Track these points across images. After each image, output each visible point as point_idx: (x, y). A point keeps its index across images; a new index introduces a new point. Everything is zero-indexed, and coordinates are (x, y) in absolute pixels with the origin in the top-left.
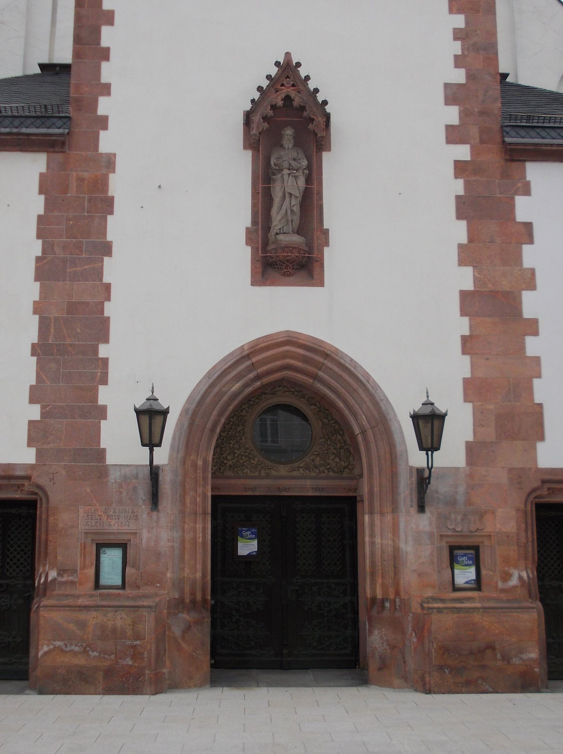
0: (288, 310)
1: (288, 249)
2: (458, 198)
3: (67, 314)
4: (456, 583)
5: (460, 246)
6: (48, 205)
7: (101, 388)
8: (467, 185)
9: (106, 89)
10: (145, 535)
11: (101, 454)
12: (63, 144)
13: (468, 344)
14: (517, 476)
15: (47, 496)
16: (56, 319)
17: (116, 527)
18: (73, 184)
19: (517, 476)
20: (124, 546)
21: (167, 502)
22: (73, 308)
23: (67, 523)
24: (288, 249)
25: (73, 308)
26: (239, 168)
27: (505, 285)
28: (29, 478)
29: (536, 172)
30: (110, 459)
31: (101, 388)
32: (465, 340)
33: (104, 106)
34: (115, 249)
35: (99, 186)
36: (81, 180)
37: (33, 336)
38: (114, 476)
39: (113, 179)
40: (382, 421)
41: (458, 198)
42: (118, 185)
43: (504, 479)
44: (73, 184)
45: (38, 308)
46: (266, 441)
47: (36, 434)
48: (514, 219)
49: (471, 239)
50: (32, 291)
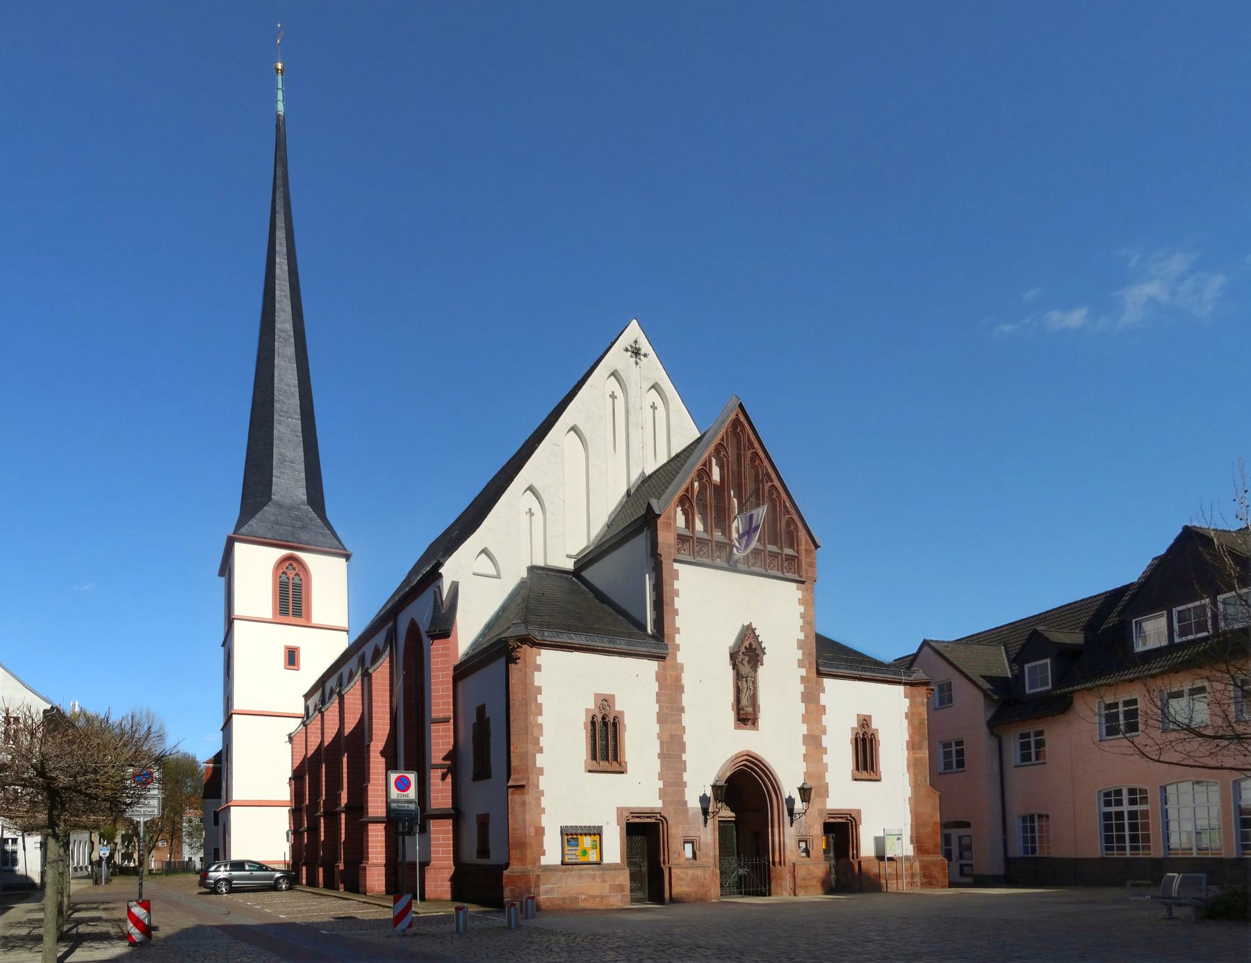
1: (746, 716)
4: (544, 652)
6: (660, 688)
9: (539, 668)
11: (685, 803)
14: (821, 812)
17: (692, 834)
19: (821, 812)
20: (692, 843)
23: (676, 832)
24: (746, 716)
25: (672, 737)
26: (729, 674)
27: (817, 733)
29: (827, 682)
30: (689, 805)
33: (678, 639)
34: (799, 680)
35: (678, 679)
38: (691, 812)
40: (777, 790)
42: (686, 679)
43: (816, 812)
45: (660, 736)
46: (1126, 703)
47: (663, 794)
50: (656, 728)
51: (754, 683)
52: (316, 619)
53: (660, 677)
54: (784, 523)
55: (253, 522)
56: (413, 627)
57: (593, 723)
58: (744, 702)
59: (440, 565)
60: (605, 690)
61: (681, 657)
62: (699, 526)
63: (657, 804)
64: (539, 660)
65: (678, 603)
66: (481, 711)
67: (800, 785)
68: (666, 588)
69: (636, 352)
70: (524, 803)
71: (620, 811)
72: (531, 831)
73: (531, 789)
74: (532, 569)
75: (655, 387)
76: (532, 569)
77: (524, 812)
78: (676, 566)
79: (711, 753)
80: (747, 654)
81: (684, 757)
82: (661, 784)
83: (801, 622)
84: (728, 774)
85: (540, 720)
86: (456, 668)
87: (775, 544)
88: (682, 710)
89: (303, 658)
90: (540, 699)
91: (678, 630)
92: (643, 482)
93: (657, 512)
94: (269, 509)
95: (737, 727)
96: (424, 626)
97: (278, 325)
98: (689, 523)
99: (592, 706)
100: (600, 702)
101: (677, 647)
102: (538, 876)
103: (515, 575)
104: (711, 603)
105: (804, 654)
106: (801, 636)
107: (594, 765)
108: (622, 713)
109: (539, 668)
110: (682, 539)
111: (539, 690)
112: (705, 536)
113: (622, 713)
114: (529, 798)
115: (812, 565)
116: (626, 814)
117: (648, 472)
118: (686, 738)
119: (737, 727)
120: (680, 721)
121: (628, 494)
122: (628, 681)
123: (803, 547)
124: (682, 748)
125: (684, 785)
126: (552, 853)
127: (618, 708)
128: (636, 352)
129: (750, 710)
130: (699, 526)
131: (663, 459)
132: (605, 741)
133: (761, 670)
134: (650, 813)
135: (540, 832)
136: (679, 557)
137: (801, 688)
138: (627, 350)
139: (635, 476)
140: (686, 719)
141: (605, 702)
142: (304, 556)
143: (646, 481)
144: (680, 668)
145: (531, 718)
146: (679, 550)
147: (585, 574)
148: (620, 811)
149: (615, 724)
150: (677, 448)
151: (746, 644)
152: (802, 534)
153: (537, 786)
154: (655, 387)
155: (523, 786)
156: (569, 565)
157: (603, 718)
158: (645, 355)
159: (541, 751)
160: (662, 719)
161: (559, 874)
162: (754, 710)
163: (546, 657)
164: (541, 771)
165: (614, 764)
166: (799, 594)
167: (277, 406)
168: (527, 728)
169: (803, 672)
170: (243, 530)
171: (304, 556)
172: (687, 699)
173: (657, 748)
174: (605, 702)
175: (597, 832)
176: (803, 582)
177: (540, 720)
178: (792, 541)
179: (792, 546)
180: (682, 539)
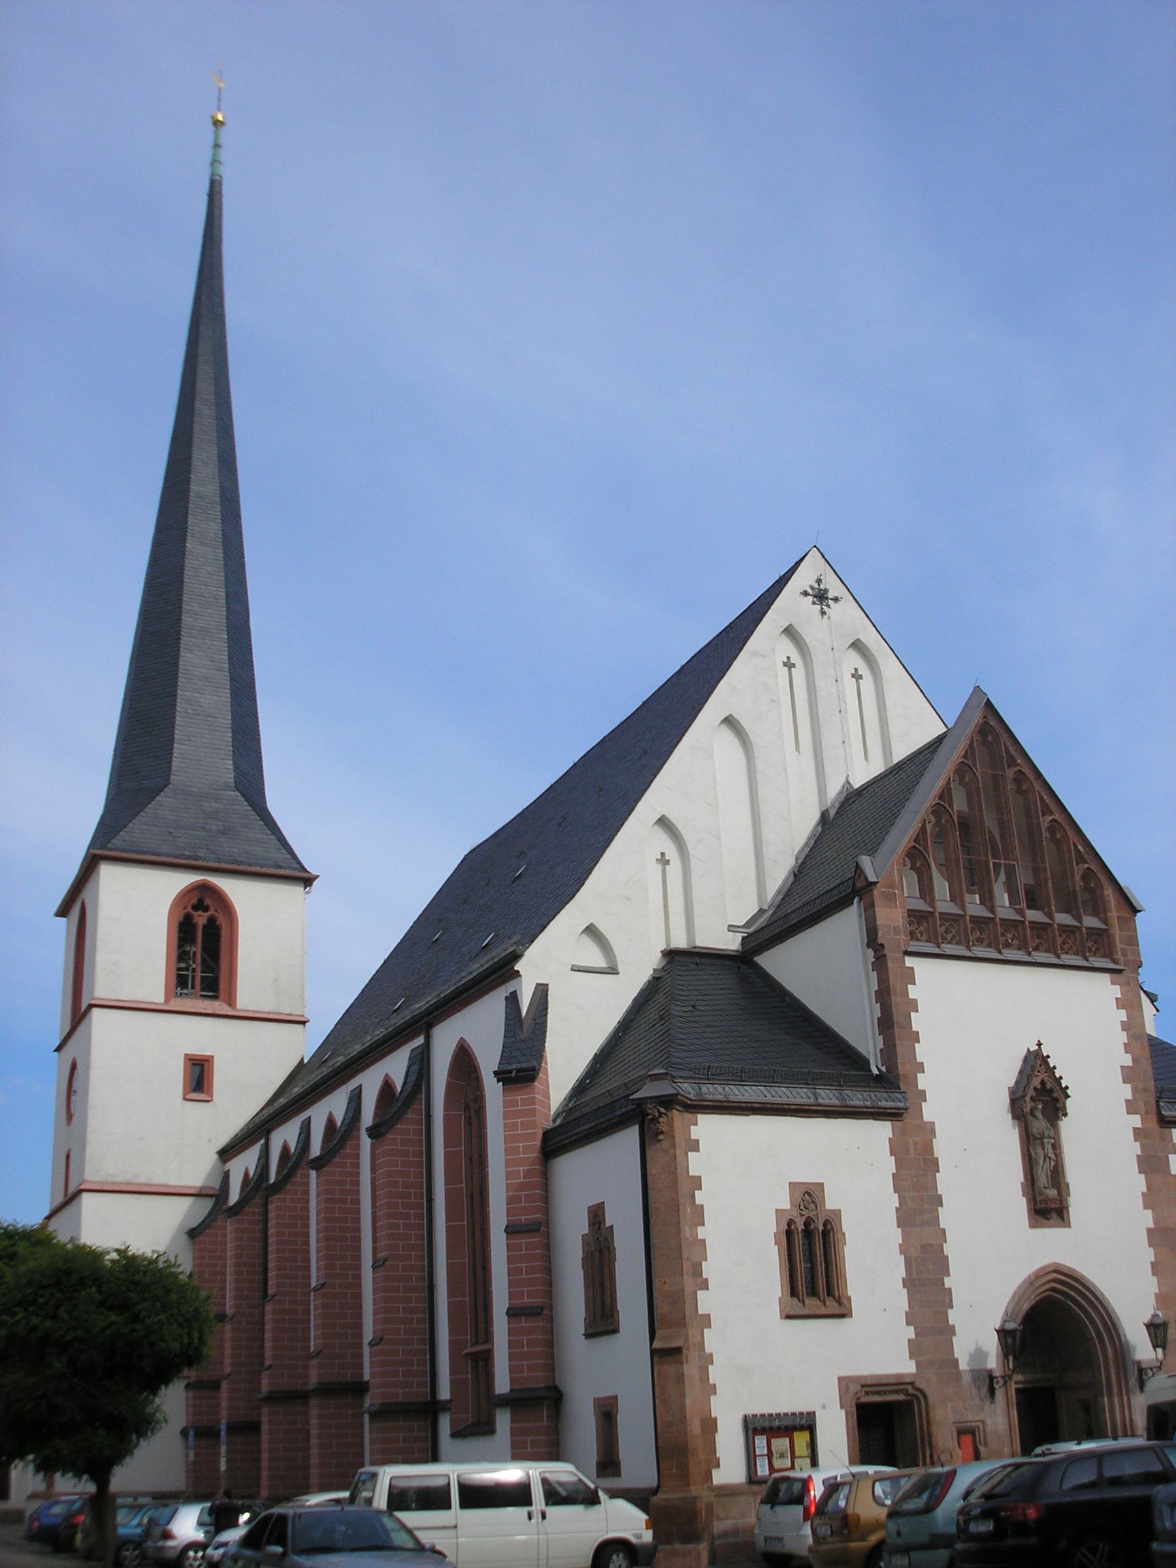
0: (1052, 1247)
1: (1047, 1204)
2: (1138, 1156)
3: (1149, 1439)
4: (701, 1118)
5: (1143, 1194)
7: (950, 1311)
8: (1142, 1146)
9: (695, 1146)
10: (989, 1422)
12: (900, 1115)
13: (1155, 1268)
15: (925, 1396)
16: (916, 1259)
17: (971, 1417)
18: (912, 1147)
21: (1000, 1394)
22: (925, 1248)
24: (1047, 1204)
25: (925, 1248)
26: (1009, 1138)
28: (912, 1383)
31: (950, 1311)
32: (1153, 1265)
33: (923, 1081)
35: (928, 1148)
36: (916, 1144)
37: (902, 1272)
39: (936, 1143)
40: (1111, 1327)
41: (1138, 1156)
42: (941, 1147)
44: (912, 1147)
45: (903, 1250)
47: (915, 1349)
48: (1169, 1172)
49: (1148, 1189)
50: (896, 1236)
51: (1056, 1146)
52: (245, 1000)
53: (897, 1148)
54: (1077, 878)
55: (135, 826)
56: (464, 1060)
57: (789, 1234)
58: (1043, 1179)
59: (516, 957)
60: (807, 1176)
61: (929, 1112)
62: (941, 887)
63: (906, 1367)
64: (695, 1132)
65: (918, 1021)
66: (597, 1215)
67: (1147, 1318)
68: (895, 999)
69: (821, 596)
70: (681, 1378)
71: (844, 1383)
72: (695, 1427)
73: (692, 1355)
74: (671, 955)
75: (857, 646)
76: (671, 955)
77: (682, 1395)
78: (909, 961)
79: (993, 1265)
80: (1038, 1097)
81: (948, 1283)
82: (911, 1332)
83: (1123, 1037)
84: (1026, 1307)
85: (701, 1232)
86: (547, 1135)
87: (1067, 911)
88: (939, 1201)
89: (220, 1077)
90: (700, 1197)
91: (921, 1067)
92: (847, 799)
93: (872, 878)
94: (165, 800)
95: (1033, 1225)
96: (488, 1059)
97: (194, 488)
98: (926, 890)
99: (786, 1205)
100: (798, 1196)
101: (922, 1095)
102: (710, 1506)
103: (639, 967)
104: (972, 1020)
105: (1135, 1091)
106: (1127, 1060)
107: (796, 1306)
108: (837, 1213)
109: (695, 1146)
110: (915, 916)
111: (697, 1183)
112: (954, 909)
113: (837, 1213)
114: (690, 1369)
115: (1133, 941)
116: (854, 1388)
117: (857, 783)
118: (948, 1249)
119: (1033, 1225)
120: (936, 1220)
121: (824, 815)
122: (847, 1160)
123: (1113, 914)
124: (943, 1266)
125: (952, 1330)
126: (730, 1468)
127: (830, 1205)
128: (821, 596)
129: (1053, 1193)
130: (941, 887)
131: (877, 767)
132: (811, 1262)
133: (1064, 1124)
134: (898, 1384)
135: (710, 1426)
136: (915, 946)
137: (1137, 1148)
138: (806, 594)
139: (834, 789)
140: (947, 1217)
141: (808, 1195)
142: (229, 886)
143: (852, 798)
144: (930, 1129)
145: (687, 1231)
146: (913, 936)
147: (765, 960)
148: (844, 1383)
149: (825, 1233)
150: (900, 752)
151: (1036, 1082)
152: (1109, 892)
153: (702, 1346)
154: (857, 646)
155: (678, 1350)
156: (732, 943)
157: (807, 1224)
158: (836, 600)
159: (705, 1285)
160: (905, 1219)
161: (742, 1500)
162: (1060, 1194)
163: (708, 1129)
164: (706, 1321)
165: (830, 1302)
166: (1116, 991)
167: (186, 619)
168: (680, 1247)
169: (1136, 1121)
170: (117, 842)
171: (229, 886)
172: (945, 1182)
173: (900, 1271)
174: (808, 1195)
175: (806, 1424)
176: (1119, 971)
177: (701, 1232)
178: (1098, 909)
179: (1095, 913)
180: (915, 916)
